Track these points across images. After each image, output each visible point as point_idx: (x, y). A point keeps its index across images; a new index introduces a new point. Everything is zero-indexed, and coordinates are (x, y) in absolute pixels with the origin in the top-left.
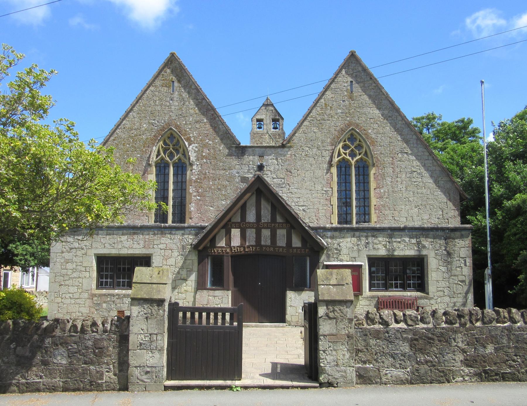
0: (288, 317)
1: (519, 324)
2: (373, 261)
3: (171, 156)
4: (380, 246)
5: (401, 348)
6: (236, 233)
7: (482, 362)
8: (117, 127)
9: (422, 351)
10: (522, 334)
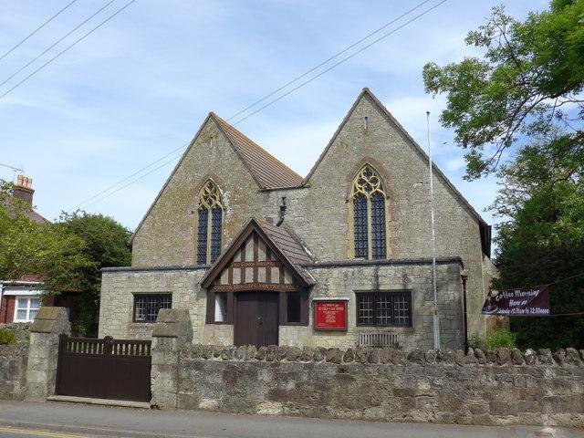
2: (361, 296)
6: (237, 272)
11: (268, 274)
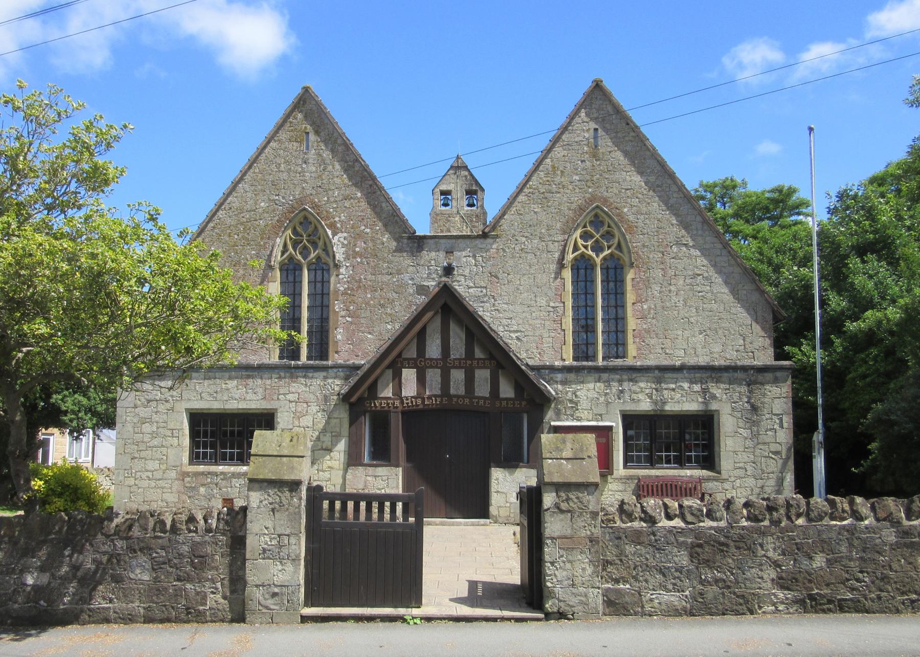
0: (493, 510)
1: (866, 522)
3: (305, 252)
4: (641, 396)
5: (675, 559)
6: (409, 376)
7: (806, 581)
8: (219, 206)
9: (708, 563)
10: (871, 537)
11: (470, 381)
